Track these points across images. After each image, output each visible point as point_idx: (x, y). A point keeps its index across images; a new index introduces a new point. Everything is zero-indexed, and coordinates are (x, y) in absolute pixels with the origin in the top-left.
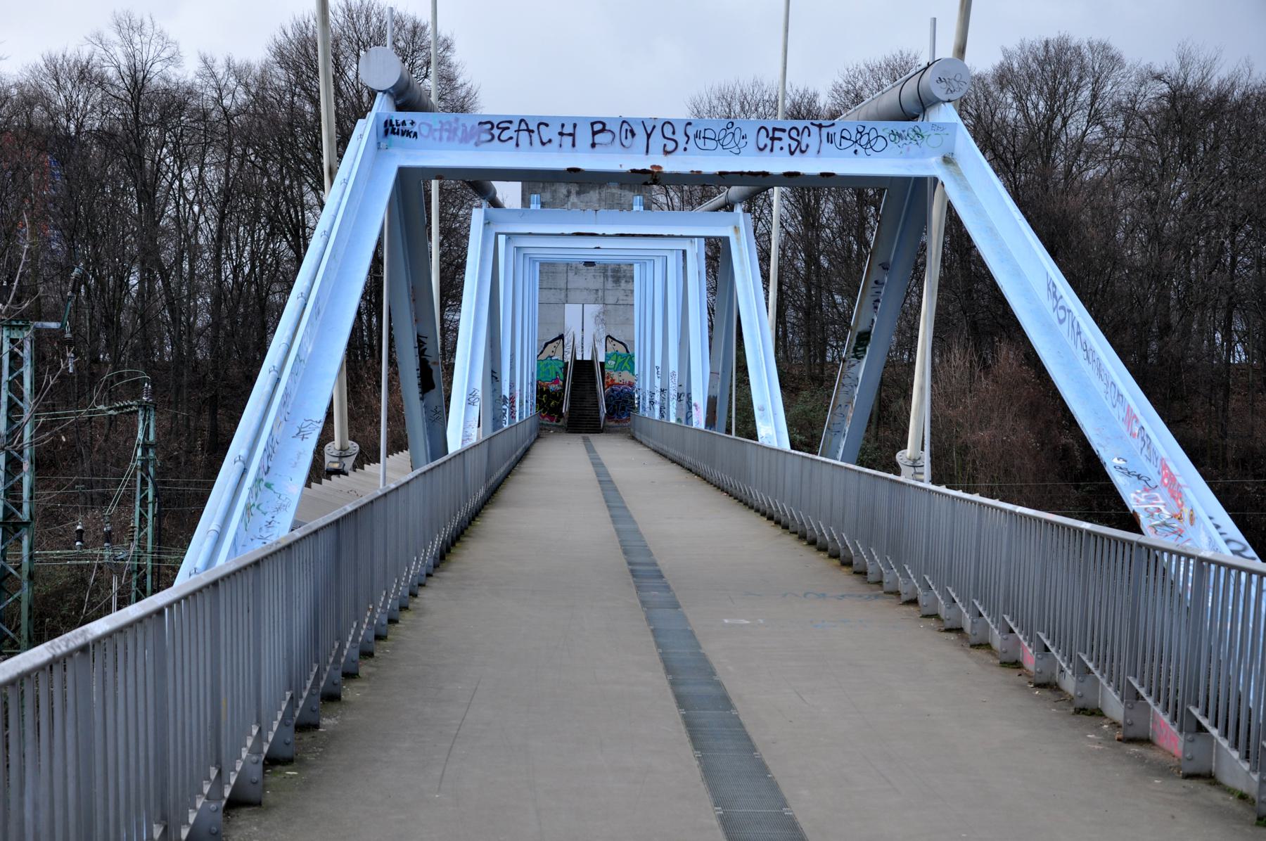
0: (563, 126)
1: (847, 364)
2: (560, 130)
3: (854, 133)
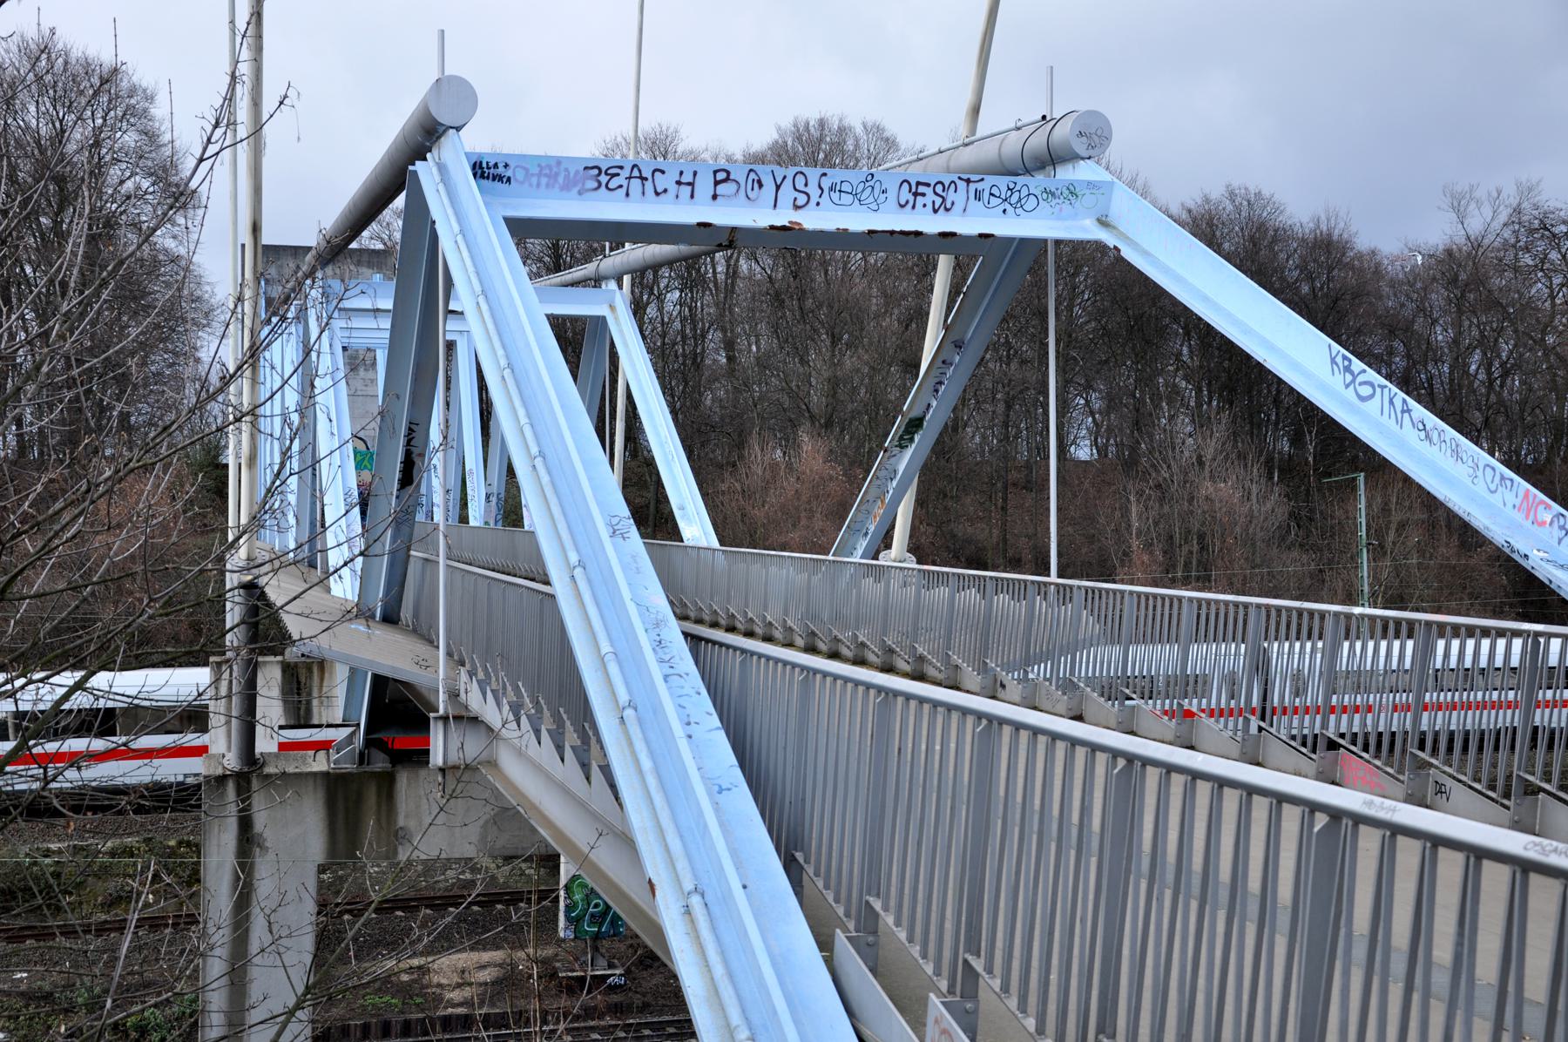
0: (681, 173)
1: (887, 454)
2: (678, 179)
3: (1004, 189)
